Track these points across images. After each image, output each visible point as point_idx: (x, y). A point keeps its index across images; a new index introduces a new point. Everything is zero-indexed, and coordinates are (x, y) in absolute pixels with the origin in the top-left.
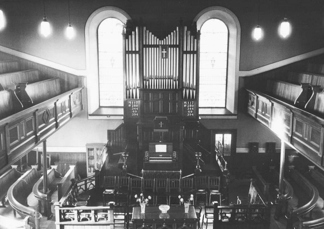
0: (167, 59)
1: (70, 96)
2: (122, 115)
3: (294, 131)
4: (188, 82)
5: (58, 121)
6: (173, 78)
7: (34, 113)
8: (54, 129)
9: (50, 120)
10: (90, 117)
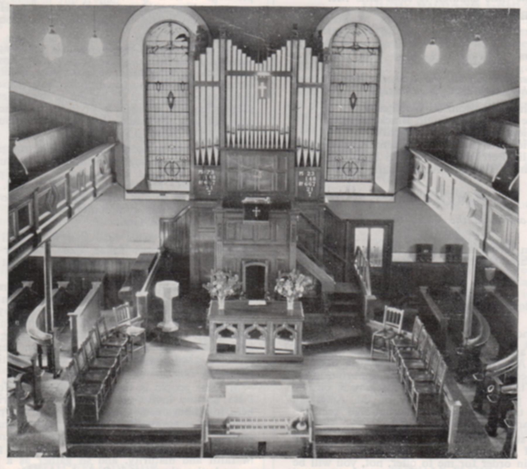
0: (269, 100)
1: (93, 161)
2: (187, 193)
3: (489, 229)
4: (306, 137)
5: (72, 205)
6: (279, 131)
7: (32, 196)
8: (66, 219)
9: (59, 205)
10: (129, 196)
